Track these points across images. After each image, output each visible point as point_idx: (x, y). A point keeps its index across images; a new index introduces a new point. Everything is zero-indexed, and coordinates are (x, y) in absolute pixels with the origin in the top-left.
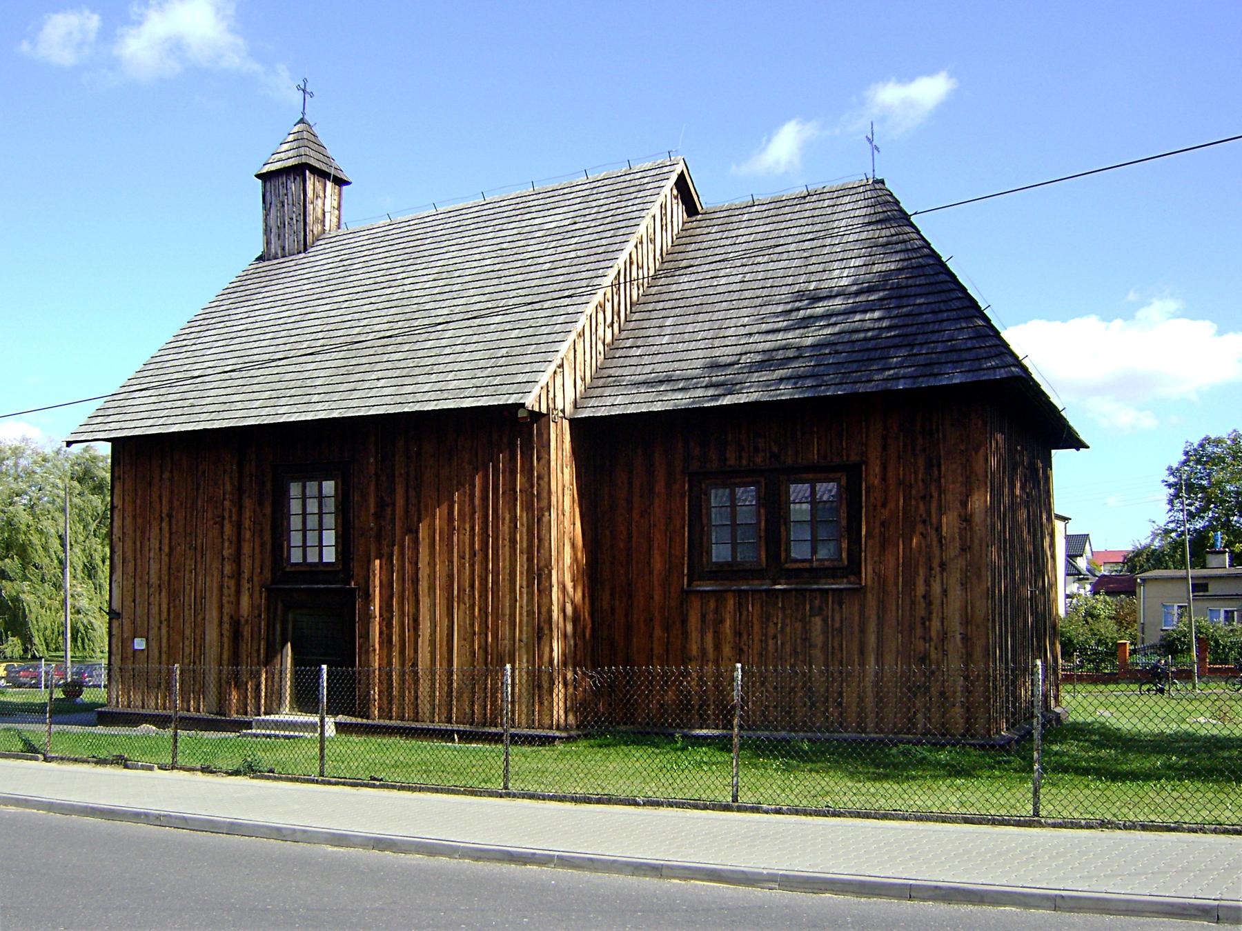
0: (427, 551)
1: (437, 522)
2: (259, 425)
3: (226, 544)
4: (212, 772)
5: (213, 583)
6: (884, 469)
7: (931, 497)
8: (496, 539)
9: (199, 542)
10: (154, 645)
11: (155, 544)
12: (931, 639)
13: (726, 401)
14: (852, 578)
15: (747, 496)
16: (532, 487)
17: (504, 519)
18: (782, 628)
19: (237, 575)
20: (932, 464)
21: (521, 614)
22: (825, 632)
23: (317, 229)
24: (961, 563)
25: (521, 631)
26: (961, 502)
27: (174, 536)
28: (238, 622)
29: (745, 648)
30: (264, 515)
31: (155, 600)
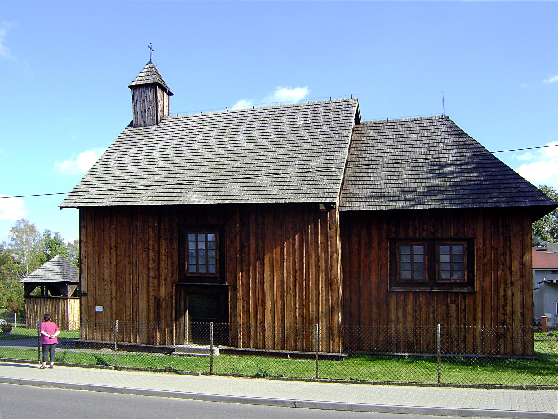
0: (269, 269)
1: (274, 256)
2: (148, 205)
3: (151, 262)
4: (240, 376)
5: (143, 281)
6: (484, 240)
7: (506, 254)
8: (308, 265)
9: (134, 260)
10: (108, 310)
11: (107, 260)
12: (507, 314)
13: (419, 207)
14: (469, 288)
15: (419, 250)
16: (327, 241)
17: (312, 256)
18: (437, 308)
19: (158, 277)
20: (507, 240)
21: (322, 300)
22: (457, 311)
23: (162, 115)
24: (520, 282)
25: (322, 308)
26: (520, 256)
27: (118, 257)
28: (159, 300)
29: (419, 317)
30: (173, 249)
31: (108, 288)
